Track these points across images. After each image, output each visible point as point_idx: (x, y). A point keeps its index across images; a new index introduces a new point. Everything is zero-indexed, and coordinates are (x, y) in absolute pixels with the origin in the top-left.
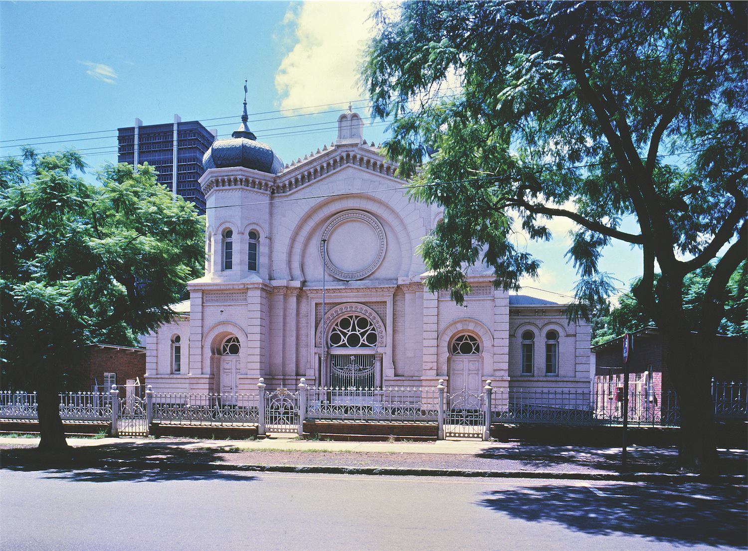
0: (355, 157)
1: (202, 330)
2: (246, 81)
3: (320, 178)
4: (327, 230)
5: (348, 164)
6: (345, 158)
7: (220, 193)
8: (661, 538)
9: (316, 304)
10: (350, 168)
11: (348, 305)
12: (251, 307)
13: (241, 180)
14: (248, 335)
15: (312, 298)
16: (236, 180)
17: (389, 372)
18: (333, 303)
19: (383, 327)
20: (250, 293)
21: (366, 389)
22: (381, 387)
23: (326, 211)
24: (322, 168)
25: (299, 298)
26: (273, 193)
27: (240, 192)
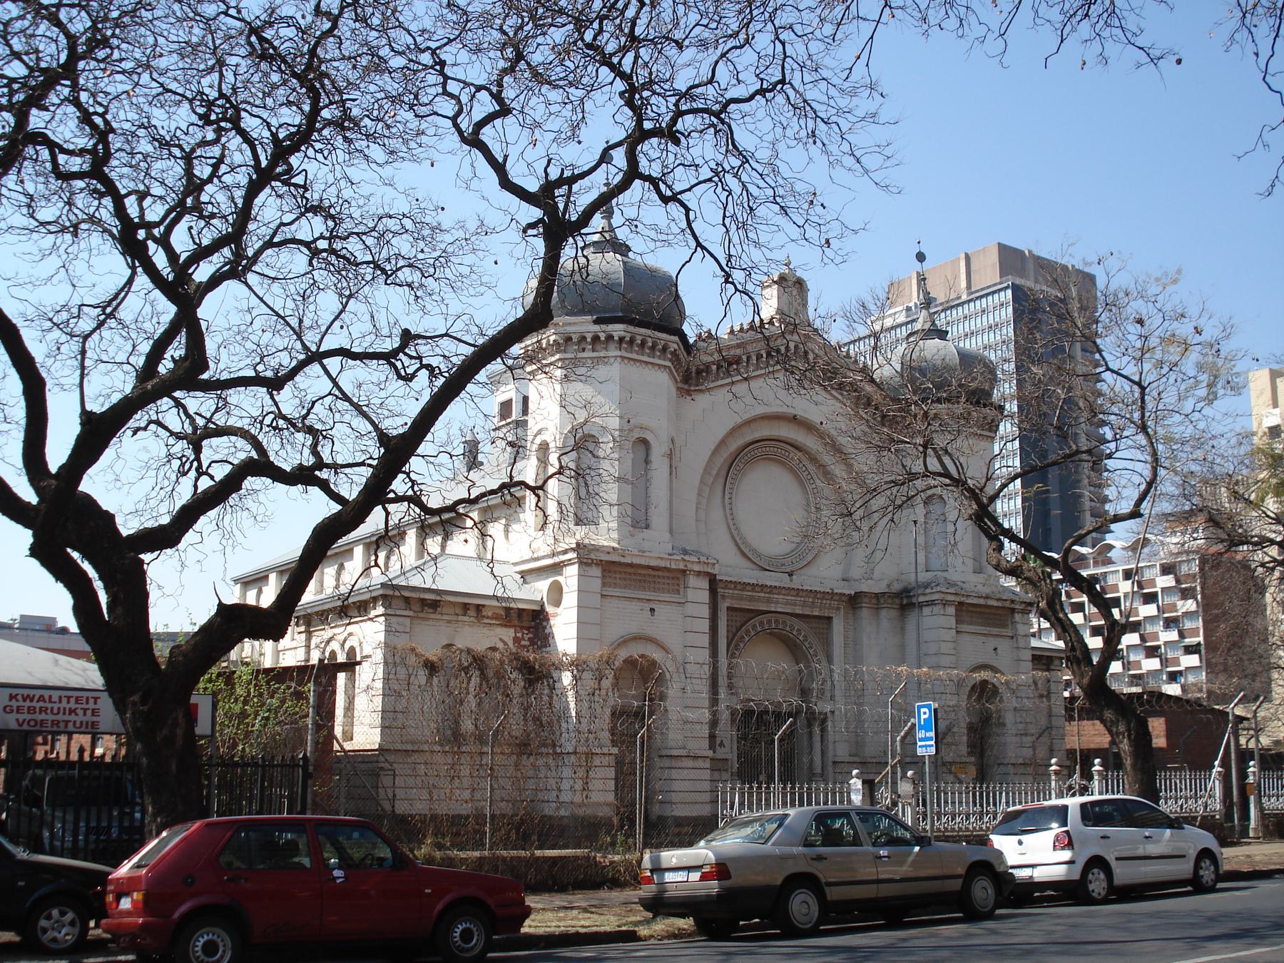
11: (773, 617)
12: (690, 609)
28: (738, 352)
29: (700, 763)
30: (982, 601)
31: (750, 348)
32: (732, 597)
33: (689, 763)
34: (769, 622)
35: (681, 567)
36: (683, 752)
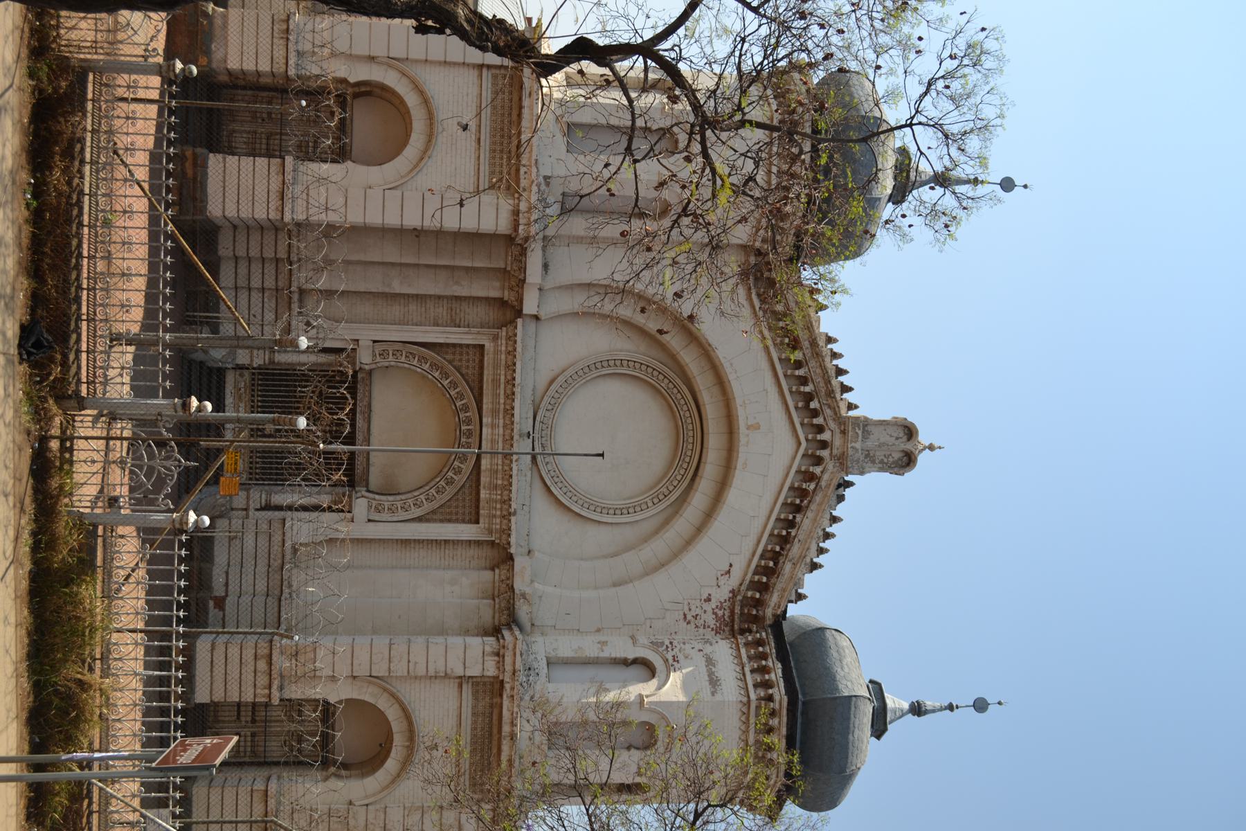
0: (819, 461)
1: (416, 61)
2: (1025, 186)
3: (775, 356)
4: (661, 377)
5: (804, 444)
6: (819, 437)
7: (738, 724)
8: (323, 358)
9: (482, 346)
10: (795, 446)
13: (770, 698)
14: (398, 193)
15: (495, 338)
16: (798, 509)
17: (302, 529)
18: (481, 388)
19: (417, 512)
20: (506, 205)
21: (182, 568)
22: (268, 507)
23: (712, 410)
24: (804, 381)
25: (502, 303)
26: (759, 253)
27: (741, 698)
28: (806, 344)
29: (274, 203)
30: (506, 729)
31: (812, 364)
32: (496, 352)
33: (275, 185)
34: (469, 421)
35: (523, 183)
36: (289, 177)
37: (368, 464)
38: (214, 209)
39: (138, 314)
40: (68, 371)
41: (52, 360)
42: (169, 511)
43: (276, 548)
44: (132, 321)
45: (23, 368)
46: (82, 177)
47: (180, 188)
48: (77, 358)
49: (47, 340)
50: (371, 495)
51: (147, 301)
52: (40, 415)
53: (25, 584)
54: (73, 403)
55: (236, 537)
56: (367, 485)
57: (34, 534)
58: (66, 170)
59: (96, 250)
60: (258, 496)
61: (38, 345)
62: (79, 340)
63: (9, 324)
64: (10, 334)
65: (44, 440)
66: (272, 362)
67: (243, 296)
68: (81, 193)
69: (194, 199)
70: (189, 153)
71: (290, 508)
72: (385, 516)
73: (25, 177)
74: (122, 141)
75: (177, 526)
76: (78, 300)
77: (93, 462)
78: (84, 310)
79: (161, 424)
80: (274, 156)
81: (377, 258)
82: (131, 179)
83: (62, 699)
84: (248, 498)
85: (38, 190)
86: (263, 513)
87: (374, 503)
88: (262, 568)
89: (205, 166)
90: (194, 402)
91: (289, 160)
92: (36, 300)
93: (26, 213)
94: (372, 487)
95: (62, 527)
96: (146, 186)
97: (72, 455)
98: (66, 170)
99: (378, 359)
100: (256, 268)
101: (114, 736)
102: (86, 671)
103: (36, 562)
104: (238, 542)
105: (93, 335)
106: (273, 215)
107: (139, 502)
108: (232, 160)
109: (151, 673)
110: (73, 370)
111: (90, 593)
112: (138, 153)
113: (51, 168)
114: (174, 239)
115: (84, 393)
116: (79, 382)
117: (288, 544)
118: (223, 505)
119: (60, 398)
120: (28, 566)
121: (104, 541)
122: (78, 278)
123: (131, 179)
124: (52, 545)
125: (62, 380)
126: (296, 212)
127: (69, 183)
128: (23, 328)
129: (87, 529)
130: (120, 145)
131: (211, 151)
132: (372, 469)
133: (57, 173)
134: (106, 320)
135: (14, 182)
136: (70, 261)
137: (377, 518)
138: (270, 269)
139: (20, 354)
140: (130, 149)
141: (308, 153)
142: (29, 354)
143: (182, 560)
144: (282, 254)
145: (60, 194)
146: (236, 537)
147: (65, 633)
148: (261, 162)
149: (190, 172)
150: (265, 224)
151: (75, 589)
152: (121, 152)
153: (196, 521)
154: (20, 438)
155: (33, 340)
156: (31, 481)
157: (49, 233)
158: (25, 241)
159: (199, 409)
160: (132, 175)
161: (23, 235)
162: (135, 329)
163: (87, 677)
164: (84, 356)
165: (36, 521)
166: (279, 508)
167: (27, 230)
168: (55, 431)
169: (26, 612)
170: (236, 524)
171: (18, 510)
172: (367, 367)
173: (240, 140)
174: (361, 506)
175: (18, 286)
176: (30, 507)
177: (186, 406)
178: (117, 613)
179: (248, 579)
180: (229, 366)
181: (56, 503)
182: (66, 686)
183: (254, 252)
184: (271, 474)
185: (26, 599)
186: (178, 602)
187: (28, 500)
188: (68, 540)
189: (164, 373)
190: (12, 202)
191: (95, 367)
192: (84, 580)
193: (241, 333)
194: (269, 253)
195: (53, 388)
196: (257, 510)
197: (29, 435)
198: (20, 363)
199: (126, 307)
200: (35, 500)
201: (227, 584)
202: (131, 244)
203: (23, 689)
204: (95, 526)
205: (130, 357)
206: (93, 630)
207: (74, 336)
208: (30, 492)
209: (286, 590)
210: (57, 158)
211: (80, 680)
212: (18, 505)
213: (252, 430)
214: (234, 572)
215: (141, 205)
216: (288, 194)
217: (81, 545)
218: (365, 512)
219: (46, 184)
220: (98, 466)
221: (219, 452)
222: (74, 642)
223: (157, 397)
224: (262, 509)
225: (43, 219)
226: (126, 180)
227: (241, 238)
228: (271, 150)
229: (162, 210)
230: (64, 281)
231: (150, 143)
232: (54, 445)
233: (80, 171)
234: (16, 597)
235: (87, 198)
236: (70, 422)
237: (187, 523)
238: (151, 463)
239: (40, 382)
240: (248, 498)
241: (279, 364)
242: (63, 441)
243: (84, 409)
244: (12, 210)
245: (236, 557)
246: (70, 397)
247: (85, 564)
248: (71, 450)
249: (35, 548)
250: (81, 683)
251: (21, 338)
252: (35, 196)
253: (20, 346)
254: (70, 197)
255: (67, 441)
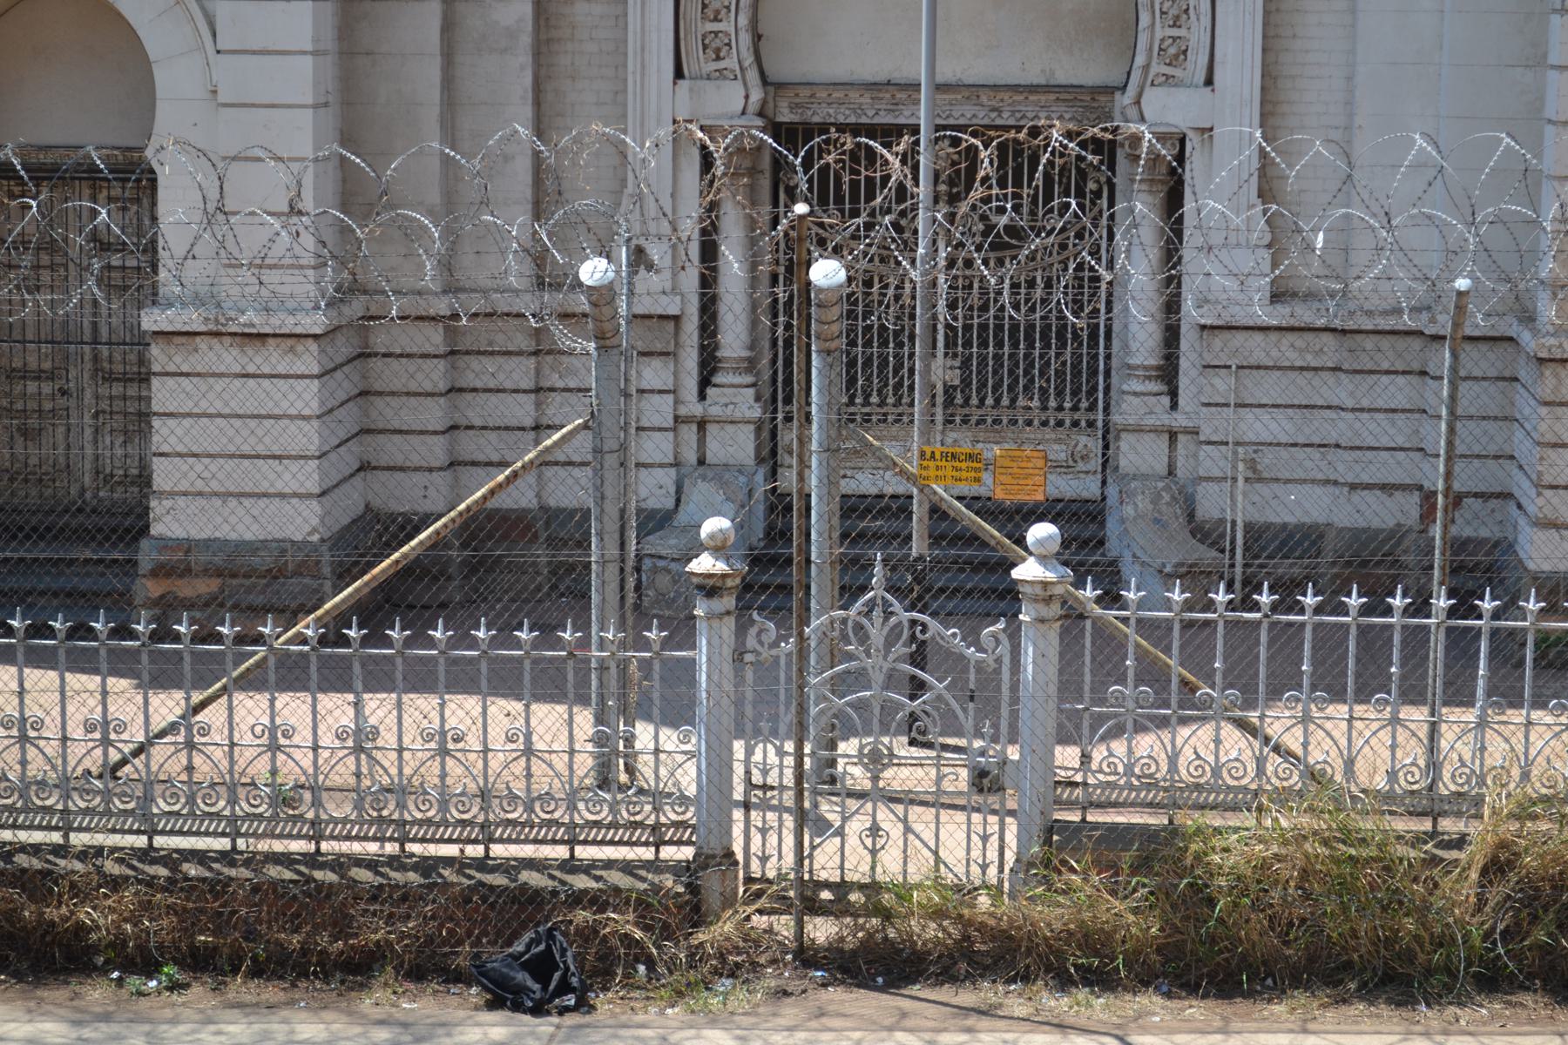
17: (1227, 275)
22: (1168, 373)
29: (272, 359)
33: (229, 358)
36: (192, 319)
37: (1047, 88)
38: (301, 522)
39: (548, 719)
40: (617, 890)
41: (588, 934)
42: (1014, 633)
43: (1287, 350)
44: (561, 731)
45: (604, 1003)
46: (99, 851)
47: (224, 612)
48: (589, 868)
49: (525, 941)
50: (1136, 77)
51: (343, 686)
52: (736, 965)
53: (1196, 1010)
54: (711, 882)
55: (1252, 465)
56: (1109, 90)
57: (1064, 982)
58: (79, 891)
59: (295, 819)
60: (1135, 402)
61: (542, 966)
62: (200, 857)
63: (473, 1034)
64: (498, 1033)
65: (807, 957)
66: (751, 365)
67: (470, 445)
68: (147, 855)
69: (276, 574)
70: (154, 588)
71: (1172, 306)
72: (1197, 35)
73: (97, 993)
74: (86, 756)
75: (1056, 609)
76: (427, 866)
77: (875, 830)
78: (451, 850)
79: (766, 654)
80: (142, 361)
81: (432, 72)
82: (185, 727)
83: (1535, 919)
84: (1138, 430)
85: (138, 961)
86: (1183, 382)
87: (1157, 68)
88: (1341, 390)
89: (188, 545)
90: (704, 564)
91: (152, 320)
92: (427, 968)
93: (196, 990)
94: (1115, 78)
95: (1050, 915)
96: (197, 697)
97: (827, 885)
98: (79, 891)
99: (731, 63)
100: (475, 410)
101: (1216, 772)
102: (1462, 856)
103: (1144, 979)
104: (1267, 459)
105: (600, 831)
106: (308, 360)
107: (989, 709)
108: (164, 474)
109: (1480, 692)
110: (617, 878)
111: (1235, 844)
112: (452, 722)
113: (81, 930)
114: (341, 619)
115: (687, 853)
116: (655, 866)
117: (1262, 313)
118: (1156, 499)
119: (695, 912)
120: (1149, 1001)
121: (1099, 806)
122: (371, 864)
123: (185, 727)
124: (1094, 941)
125: (643, 907)
126: (301, 301)
127: (116, 884)
128: (494, 1004)
129: (1055, 847)
130: (94, 762)
131: (145, 530)
132: (1062, 78)
133: (87, 914)
134: (232, 788)
135: (106, 1018)
136: (320, 886)
137: (1203, 60)
138: (479, 371)
139: (563, 1011)
140: (104, 729)
141: (135, 267)
142: (564, 988)
143: (1377, 606)
144: (434, 338)
145: (146, 906)
146: (1252, 465)
147: (1345, 909)
148: (163, 394)
149: (205, 587)
150: (344, 384)
151: (1222, 882)
152: (114, 756)
153: (1043, 559)
154: (790, 1011)
155: (523, 977)
156: (915, 990)
157: (251, 935)
158: (272, 992)
159: (719, 550)
160: (172, 728)
161: (248, 998)
162: (585, 720)
163: (1474, 856)
164: (583, 852)
165: (1026, 978)
166: (1171, 336)
167: (239, 988)
168: (784, 925)
169: (1279, 1009)
170: (1212, 461)
171: (985, 1022)
172: (756, 95)
173: (114, 451)
174: (1159, 111)
175: (378, 1013)
176: (986, 992)
177: (710, 588)
178: (1216, 772)
179: (1375, 430)
180: (761, 488)
181: (982, 927)
182: (1499, 907)
183: (434, 414)
184: (983, 360)
185: (1241, 1005)
186: (1365, 611)
187: (967, 997)
188: (1089, 900)
189: (365, 642)
190: (150, 1021)
191: (614, 825)
192: (1198, 857)
193: (582, 447)
194: (435, 375)
195: (667, 932)
196: (1174, 406)
197: (786, 993)
198: (593, 1008)
199: (361, 740)
200: (971, 978)
201: (1385, 488)
202: (23, 720)
203: (1493, 1017)
204: (1051, 828)
205: (670, 739)
206: (1347, 835)
207: (526, 876)
208: (945, 993)
209: (1407, 321)
210: (51, 913)
211: (1484, 871)
212: (971, 1021)
213: (948, 421)
214: (1345, 467)
215: (251, 708)
216: (252, 319)
217: (1100, 865)
218: (1182, 95)
219: (119, 943)
220: (884, 815)
221: (937, 512)
222: (1373, 887)
223: (692, 662)
224: (1173, 394)
225: (214, 950)
226: (190, 745)
227: (392, 449)
228: (127, 370)
229: (261, 651)
230: (374, 899)
231: (83, 683)
232: (821, 930)
233: (83, 855)
234: (1224, 1031)
235: (159, 841)
236: (758, 888)
237: (1045, 584)
238: (878, 678)
239: (651, 964)
240: (1138, 430)
241: (753, 345)
242: (812, 907)
243: (730, 854)
244: (174, 1021)
245: (1312, 463)
246: (693, 889)
247: (1153, 854)
248: (841, 888)
249: (1101, 980)
250: (1496, 867)
251: (517, 1007)
252: (150, 968)
253: (538, 1010)
254: (150, 882)
255: (807, 898)
